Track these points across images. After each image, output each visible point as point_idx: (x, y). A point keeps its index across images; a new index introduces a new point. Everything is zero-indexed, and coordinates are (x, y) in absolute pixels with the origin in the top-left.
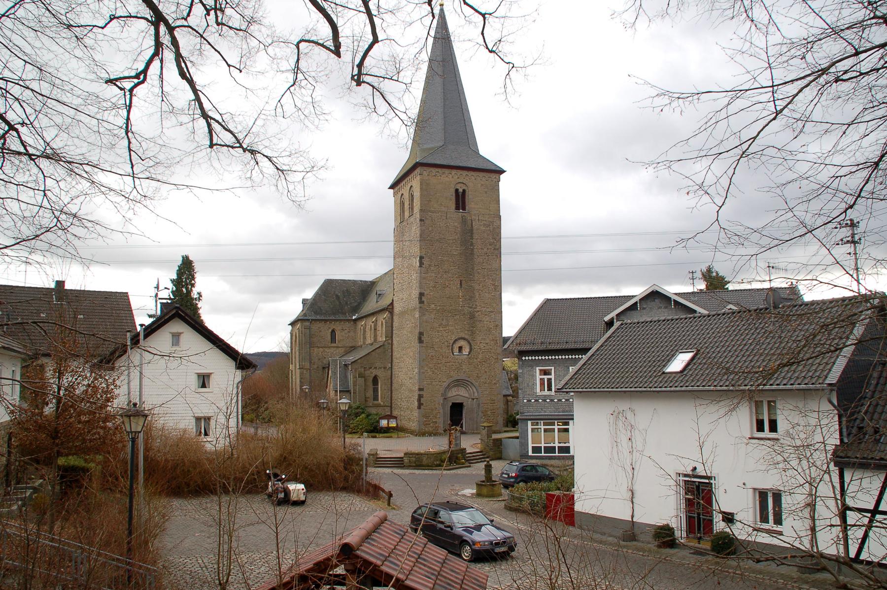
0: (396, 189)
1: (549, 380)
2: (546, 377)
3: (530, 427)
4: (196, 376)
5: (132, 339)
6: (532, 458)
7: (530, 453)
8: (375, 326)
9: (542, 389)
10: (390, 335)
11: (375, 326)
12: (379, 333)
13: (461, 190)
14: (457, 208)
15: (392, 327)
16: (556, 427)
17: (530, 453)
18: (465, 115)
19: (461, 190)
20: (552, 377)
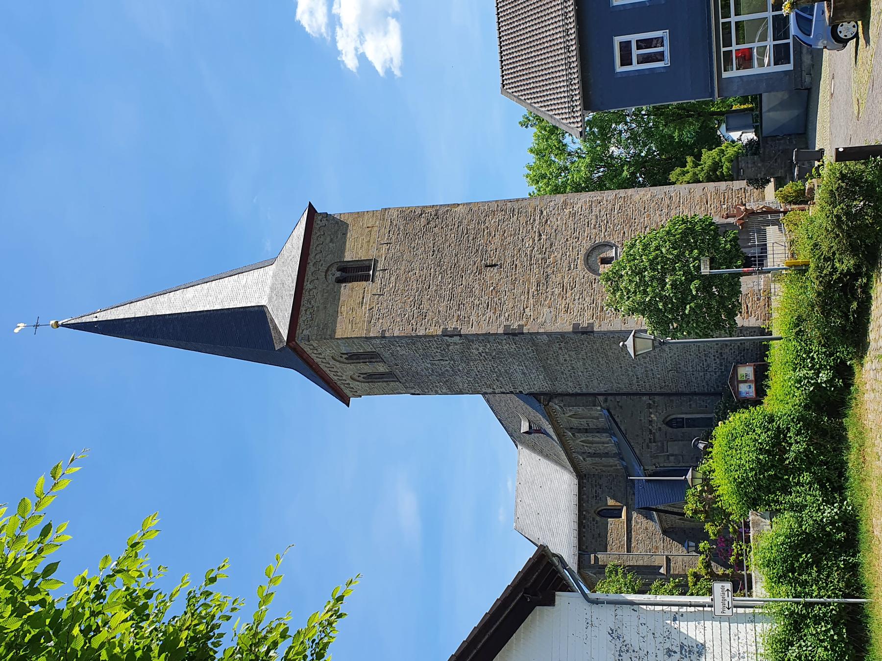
0: (347, 392)
1: (641, 44)
2: (635, 52)
3: (733, 73)
4: (531, 551)
5: (26, 506)
6: (798, 63)
7: (789, 67)
8: (579, 431)
9: (659, 57)
10: (588, 398)
11: (579, 431)
12: (601, 448)
13: (338, 274)
14: (366, 278)
15: (577, 394)
16: (733, 19)
17: (789, 67)
18: (321, 381)
19: (338, 274)
20: (634, 38)
